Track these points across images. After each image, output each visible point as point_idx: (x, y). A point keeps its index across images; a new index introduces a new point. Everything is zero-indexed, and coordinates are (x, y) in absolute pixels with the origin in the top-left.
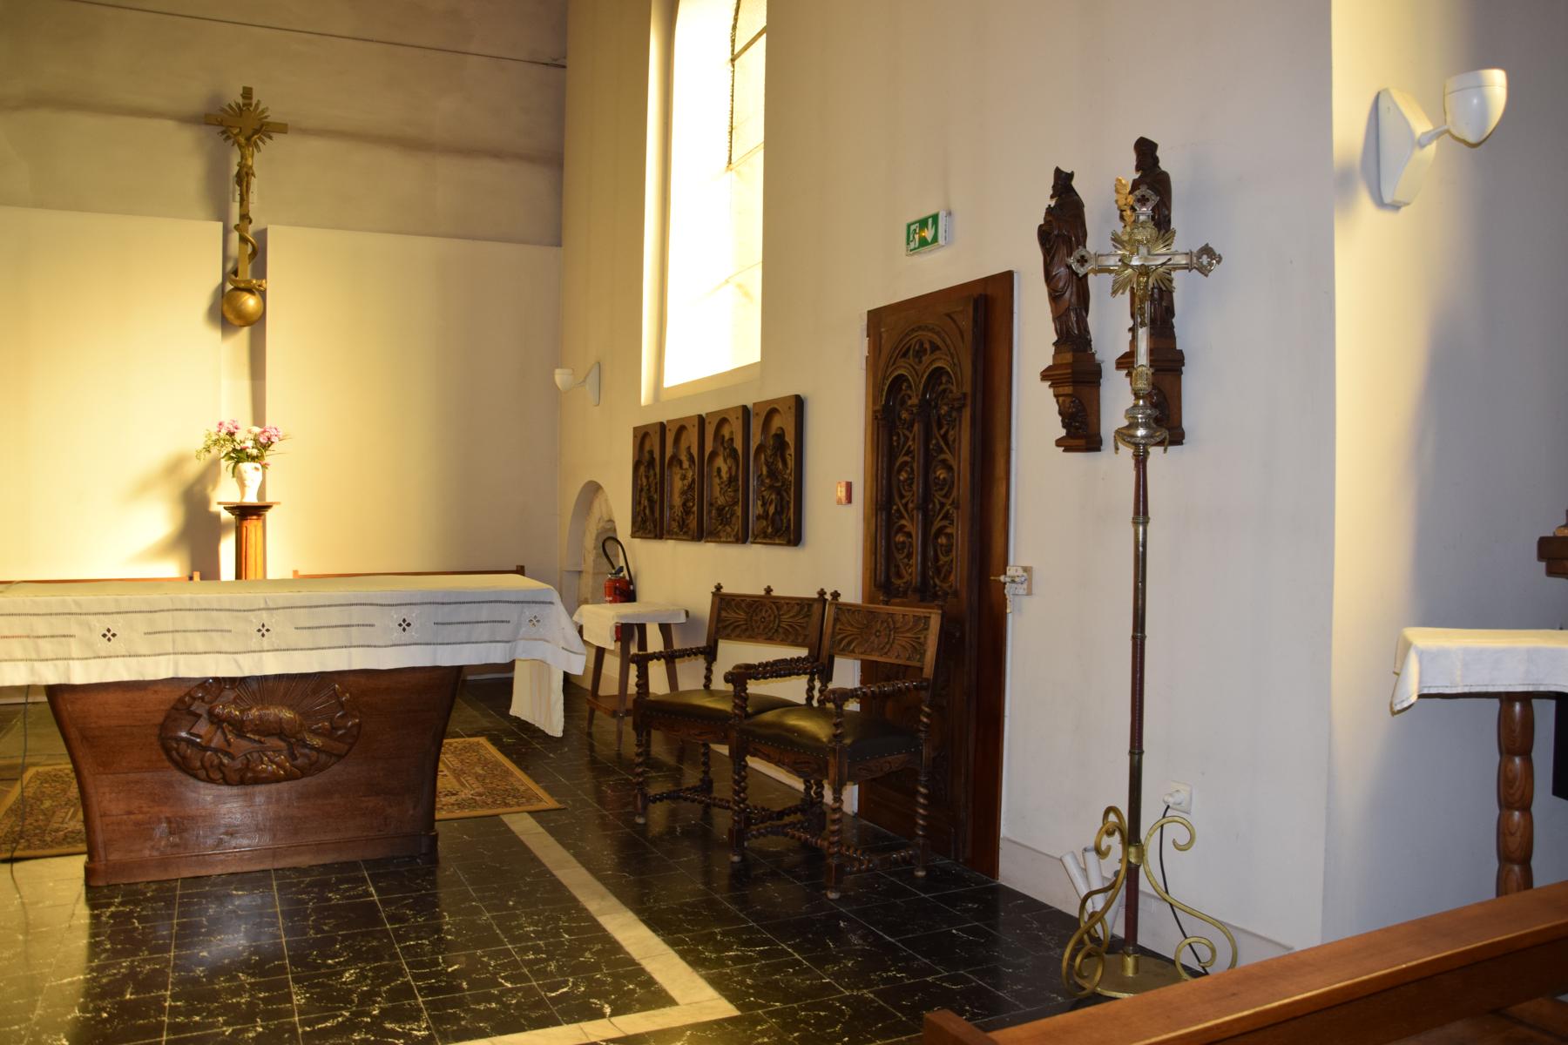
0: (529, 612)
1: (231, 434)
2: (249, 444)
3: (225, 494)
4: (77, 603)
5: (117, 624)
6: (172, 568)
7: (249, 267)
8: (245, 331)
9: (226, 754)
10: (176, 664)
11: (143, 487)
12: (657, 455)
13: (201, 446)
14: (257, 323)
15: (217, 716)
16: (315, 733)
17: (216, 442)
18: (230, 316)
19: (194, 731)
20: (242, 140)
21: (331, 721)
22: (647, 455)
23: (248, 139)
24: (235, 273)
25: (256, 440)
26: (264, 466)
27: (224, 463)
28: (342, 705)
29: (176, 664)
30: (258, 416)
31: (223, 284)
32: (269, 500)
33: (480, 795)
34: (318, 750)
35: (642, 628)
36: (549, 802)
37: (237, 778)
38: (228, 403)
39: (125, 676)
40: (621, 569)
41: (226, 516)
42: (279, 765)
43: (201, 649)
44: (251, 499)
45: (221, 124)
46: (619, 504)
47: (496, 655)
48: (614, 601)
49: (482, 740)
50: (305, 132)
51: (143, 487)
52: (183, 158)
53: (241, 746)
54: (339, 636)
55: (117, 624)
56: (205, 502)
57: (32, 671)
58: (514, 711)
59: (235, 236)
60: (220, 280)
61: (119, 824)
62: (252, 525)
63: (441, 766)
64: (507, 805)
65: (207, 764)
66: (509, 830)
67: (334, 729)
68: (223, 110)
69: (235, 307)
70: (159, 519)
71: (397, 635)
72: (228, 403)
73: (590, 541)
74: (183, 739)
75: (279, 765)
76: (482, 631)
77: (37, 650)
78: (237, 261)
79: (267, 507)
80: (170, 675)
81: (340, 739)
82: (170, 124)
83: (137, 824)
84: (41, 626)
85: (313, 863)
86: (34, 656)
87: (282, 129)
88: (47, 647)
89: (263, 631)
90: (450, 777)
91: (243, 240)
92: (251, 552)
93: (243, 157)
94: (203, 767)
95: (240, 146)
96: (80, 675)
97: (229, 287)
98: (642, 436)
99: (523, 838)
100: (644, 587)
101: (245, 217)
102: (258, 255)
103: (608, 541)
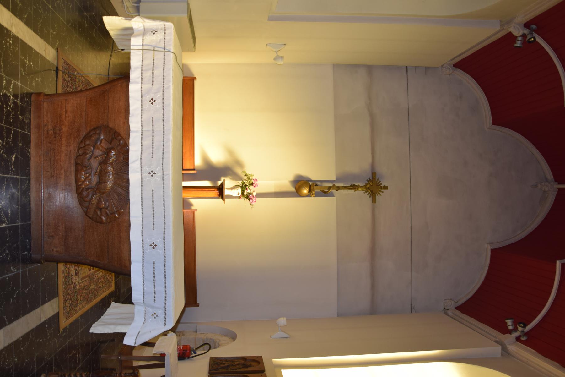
0: (160, 313)
1: (252, 184)
2: (249, 191)
3: (228, 183)
4: (168, 88)
5: (158, 105)
6: (198, 162)
7: (319, 191)
8: (294, 190)
9: (91, 157)
10: (137, 132)
11: (231, 152)
12: (250, 369)
13: (247, 173)
14: (297, 193)
15: (110, 152)
16: (99, 200)
17: (249, 178)
18: (299, 184)
19: (103, 141)
20: (368, 186)
21: (106, 208)
22: (249, 363)
23: (368, 188)
24: (316, 185)
25: (250, 194)
26: (240, 197)
27: (240, 182)
28: (113, 213)
29: (137, 132)
30: (260, 195)
31: (311, 181)
32: (226, 200)
33: (75, 287)
34: (90, 201)
35: (163, 366)
36: (64, 323)
37: (79, 162)
38: (264, 184)
39: (131, 108)
40: (195, 353)
41: (219, 183)
42: (83, 182)
43: (144, 143)
44: (226, 192)
45: (373, 178)
46: (228, 350)
47: (136, 295)
48: (179, 350)
49: (113, 288)
50: (373, 210)
51: (231, 152)
52: (359, 166)
53: (95, 164)
54: (148, 211)
55: (158, 105)
56: (225, 175)
57: (137, 68)
58: (113, 304)
59: (331, 185)
60: (313, 179)
61: (61, 107)
62: (215, 193)
63: (96, 269)
64: (65, 301)
65: (86, 147)
66: (44, 302)
67: (101, 209)
68: (378, 179)
69: (302, 186)
70: (218, 157)
71: (148, 241)
72: (264, 184)
73: (210, 336)
74: (100, 136)
75: (83, 182)
76: (149, 287)
77: (146, 70)
78: (321, 186)
79: (223, 199)
80: (131, 129)
81: (95, 212)
82: (370, 160)
83: (60, 116)
84: (158, 72)
85: (32, 199)
86: (143, 69)
87: (374, 201)
88: (148, 75)
89: (152, 173)
90: (89, 273)
91: (329, 188)
92: (204, 192)
93: (361, 187)
94: (86, 145)
95: (365, 186)
96: (134, 88)
97: (311, 183)
98: (258, 360)
99: (38, 310)
100: (186, 365)
101: (338, 188)
102: (325, 193)
103: (208, 345)
